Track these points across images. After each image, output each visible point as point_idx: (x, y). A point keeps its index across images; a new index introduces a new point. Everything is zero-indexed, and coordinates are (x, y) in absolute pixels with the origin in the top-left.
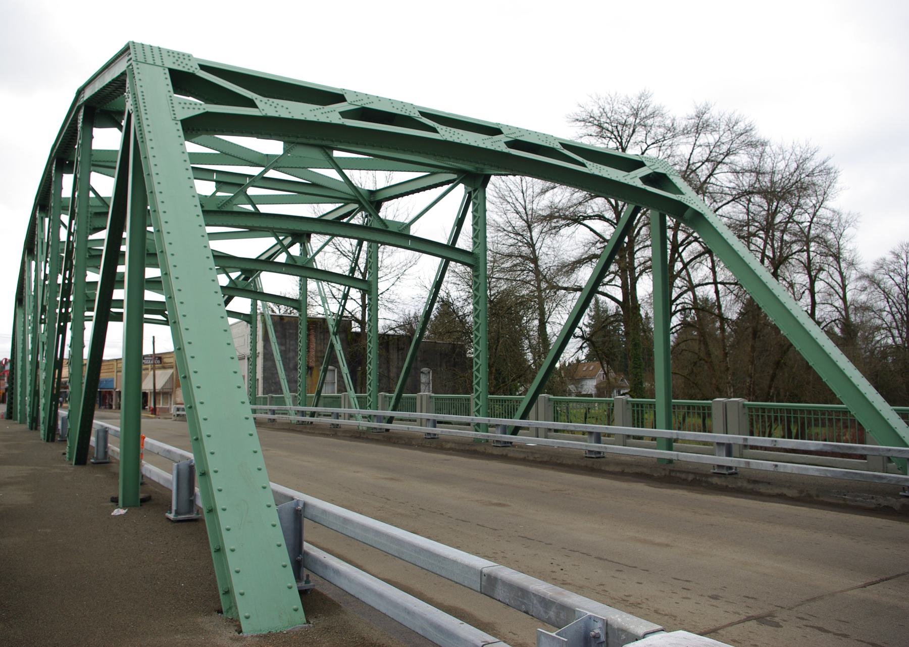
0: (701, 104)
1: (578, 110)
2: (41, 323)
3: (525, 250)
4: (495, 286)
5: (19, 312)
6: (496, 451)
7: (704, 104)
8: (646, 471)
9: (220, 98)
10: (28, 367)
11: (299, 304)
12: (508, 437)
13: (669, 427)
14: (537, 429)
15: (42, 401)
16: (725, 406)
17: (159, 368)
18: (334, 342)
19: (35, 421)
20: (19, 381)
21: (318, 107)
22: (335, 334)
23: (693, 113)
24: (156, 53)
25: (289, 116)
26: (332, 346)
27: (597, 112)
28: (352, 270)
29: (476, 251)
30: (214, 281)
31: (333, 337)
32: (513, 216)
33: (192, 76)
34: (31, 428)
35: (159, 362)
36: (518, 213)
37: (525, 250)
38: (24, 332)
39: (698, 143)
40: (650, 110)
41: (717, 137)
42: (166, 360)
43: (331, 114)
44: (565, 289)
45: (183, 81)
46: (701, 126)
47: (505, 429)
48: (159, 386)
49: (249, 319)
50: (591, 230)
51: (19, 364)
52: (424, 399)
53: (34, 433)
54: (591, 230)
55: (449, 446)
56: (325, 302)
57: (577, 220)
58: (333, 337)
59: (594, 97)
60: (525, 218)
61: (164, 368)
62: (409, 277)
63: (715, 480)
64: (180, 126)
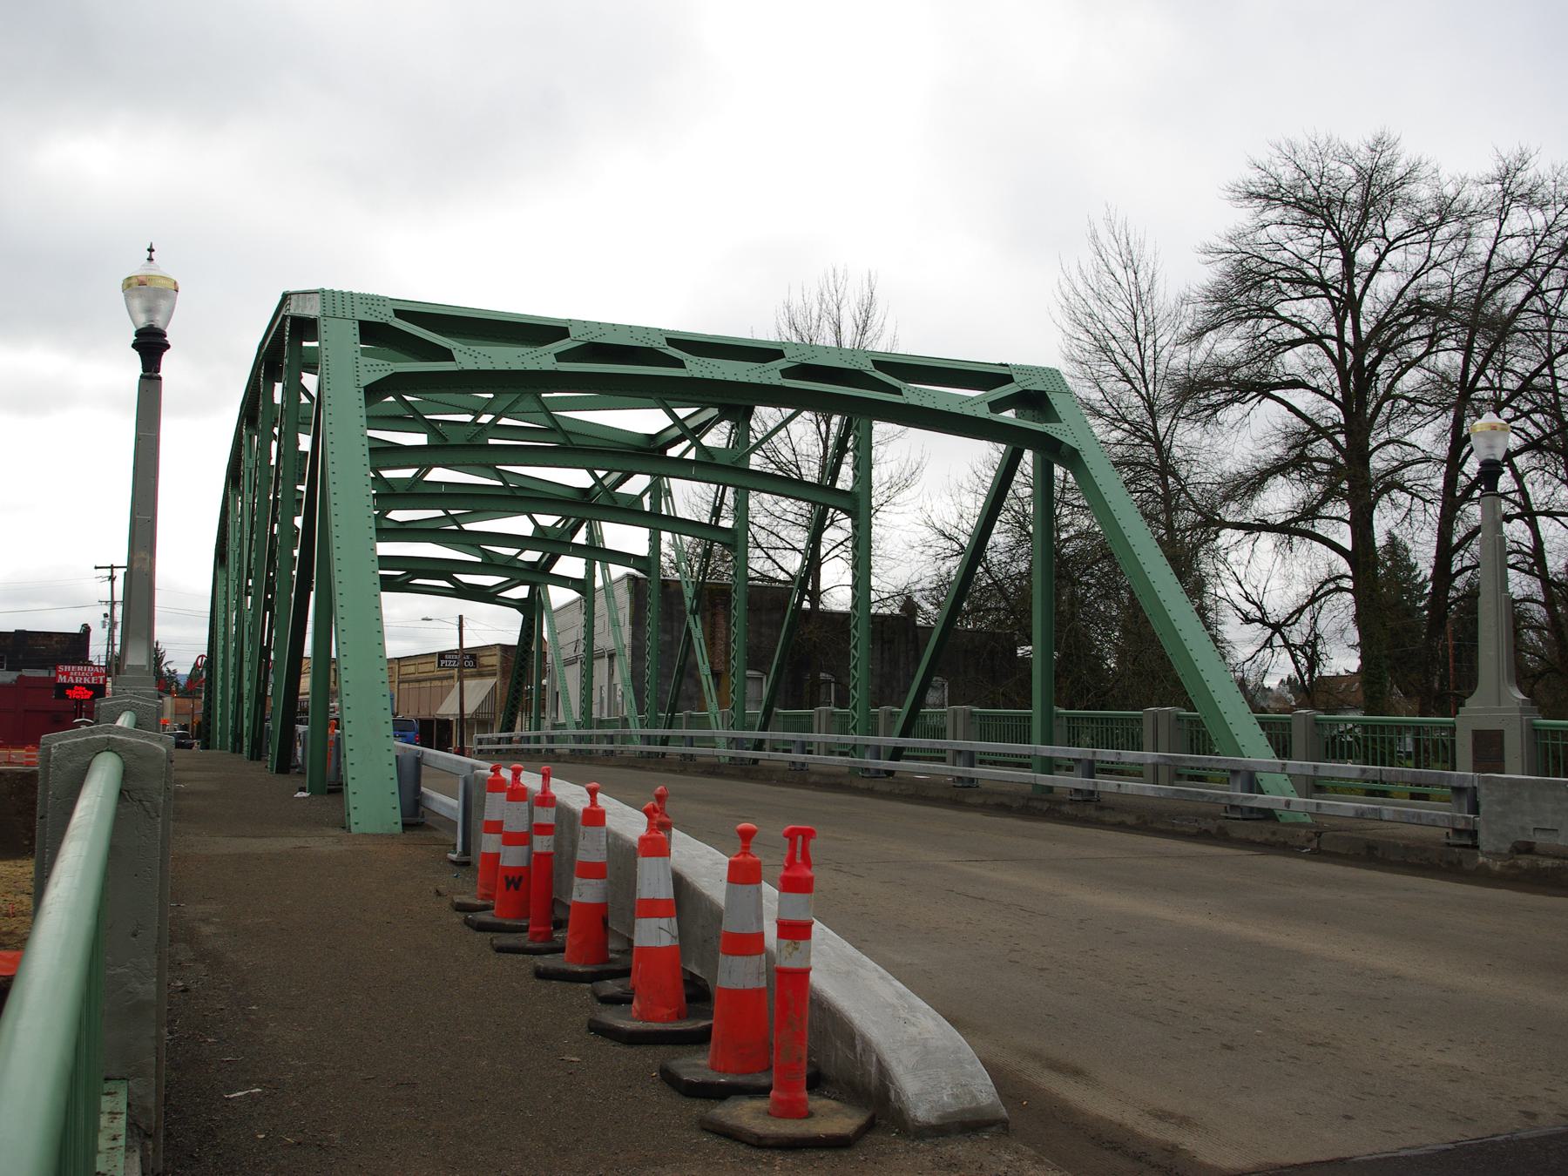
0: (1510, 152)
1: (1255, 176)
2: (247, 594)
3: (1146, 452)
4: (1070, 524)
5: (220, 574)
6: (862, 784)
7: (1516, 152)
8: (1006, 800)
9: (419, 349)
10: (231, 660)
11: (647, 563)
12: (885, 764)
13: (1048, 740)
14: (878, 747)
15: (246, 706)
16: (1155, 715)
17: (473, 676)
18: (692, 625)
19: (238, 738)
20: (219, 683)
21: (528, 350)
22: (694, 612)
23: (1491, 168)
24: (348, 299)
25: (489, 367)
26: (689, 631)
27: (1287, 175)
28: (716, 512)
29: (857, 489)
30: (374, 550)
31: (690, 618)
32: (1114, 386)
33: (385, 327)
34: (234, 751)
35: (470, 663)
36: (1129, 381)
37: (1146, 452)
38: (226, 606)
39: (1506, 230)
40: (1398, 171)
41: (1551, 214)
42: (485, 661)
43: (543, 358)
44: (1238, 526)
45: (372, 333)
46: (1512, 191)
47: (877, 752)
48: (469, 709)
49: (583, 586)
50: (1291, 408)
51: (220, 657)
52: (823, 716)
53: (237, 756)
54: (1291, 408)
55: (813, 778)
56: (776, 552)
57: (1264, 389)
58: (690, 618)
59: (1285, 148)
60: (1143, 391)
61: (480, 675)
62: (896, 509)
63: (1066, 809)
64: (362, 395)
